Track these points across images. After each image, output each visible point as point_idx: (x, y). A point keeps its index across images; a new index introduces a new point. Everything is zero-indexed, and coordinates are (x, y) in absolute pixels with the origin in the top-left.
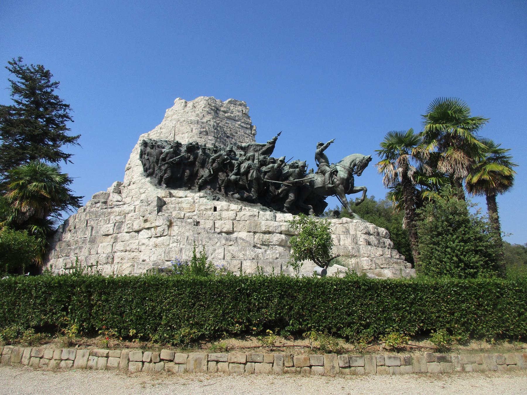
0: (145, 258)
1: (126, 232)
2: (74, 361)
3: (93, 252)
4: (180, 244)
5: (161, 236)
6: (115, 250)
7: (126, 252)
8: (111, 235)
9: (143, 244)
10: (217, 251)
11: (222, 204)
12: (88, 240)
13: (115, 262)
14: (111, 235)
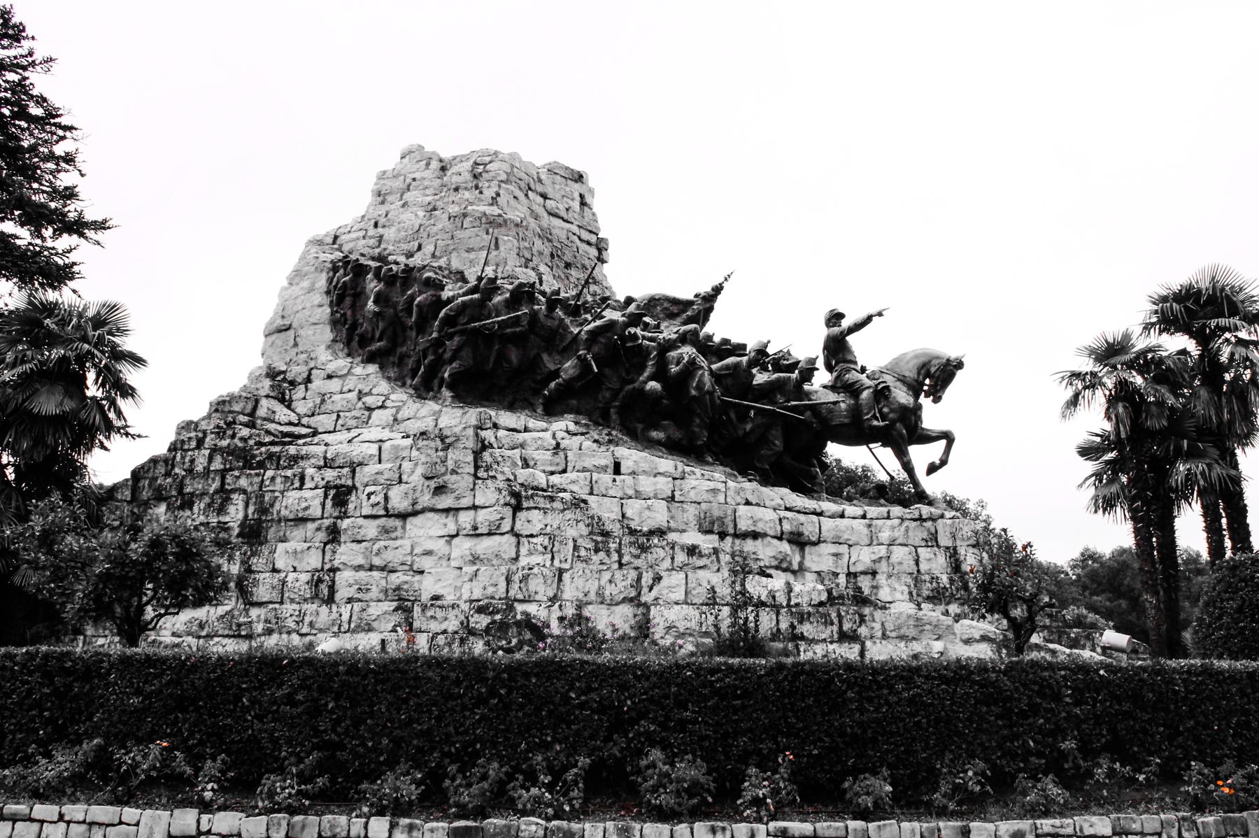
0: (440, 592)
1: (366, 517)
2: (121, 823)
3: (258, 563)
4: (553, 558)
5: (490, 534)
6: (336, 563)
7: (370, 570)
8: (314, 520)
9: (428, 553)
10: (664, 583)
11: (631, 456)
12: (237, 531)
13: (338, 597)
14: (314, 520)
